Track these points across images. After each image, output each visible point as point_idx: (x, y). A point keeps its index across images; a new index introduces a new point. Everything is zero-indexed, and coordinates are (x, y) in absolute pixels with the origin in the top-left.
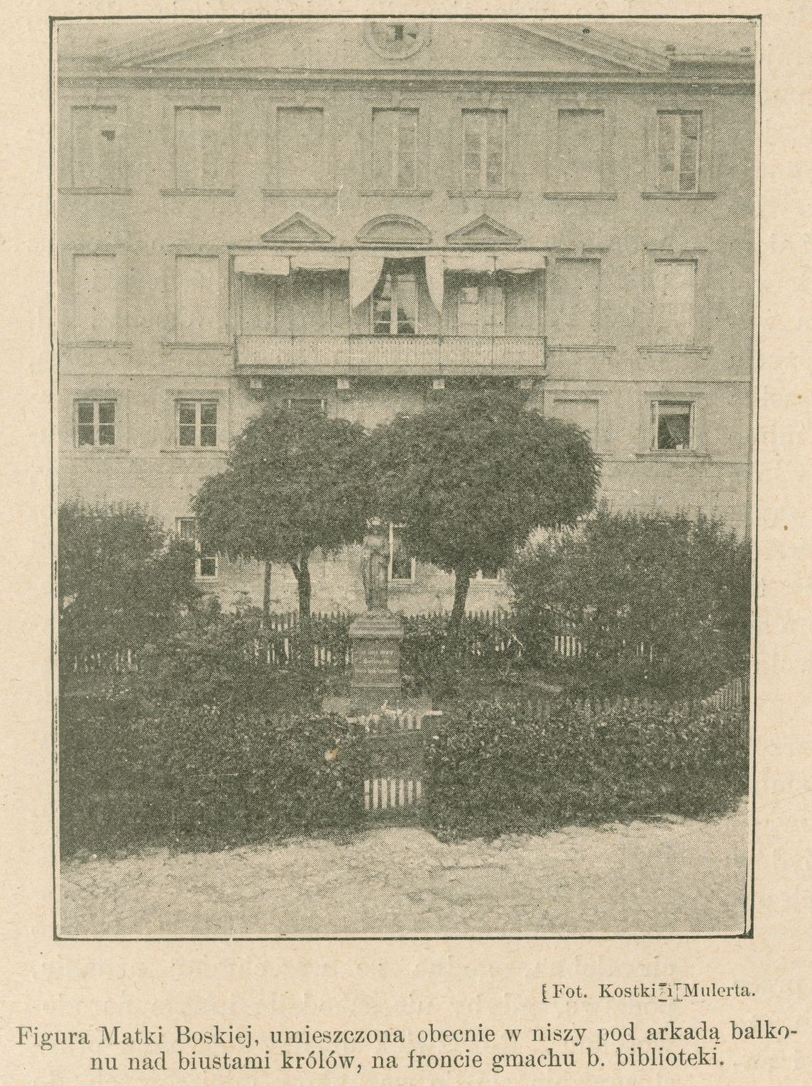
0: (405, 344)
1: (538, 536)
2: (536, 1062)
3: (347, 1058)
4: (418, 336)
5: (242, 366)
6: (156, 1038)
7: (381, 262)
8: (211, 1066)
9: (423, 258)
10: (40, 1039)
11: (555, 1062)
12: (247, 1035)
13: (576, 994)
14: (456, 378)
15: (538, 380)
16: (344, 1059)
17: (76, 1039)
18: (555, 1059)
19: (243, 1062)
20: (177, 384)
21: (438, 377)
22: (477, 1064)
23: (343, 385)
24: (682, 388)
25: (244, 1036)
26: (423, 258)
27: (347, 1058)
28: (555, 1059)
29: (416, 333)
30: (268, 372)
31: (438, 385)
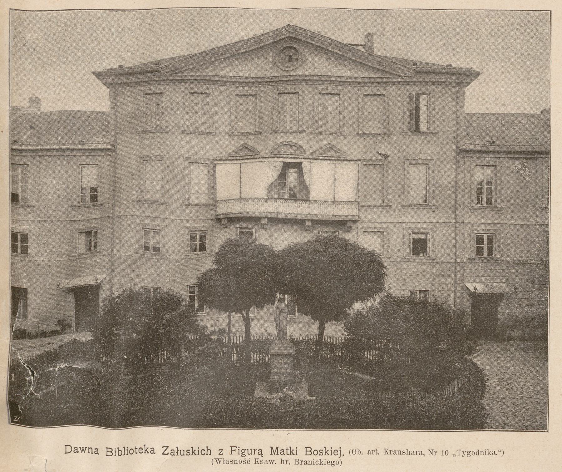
0: (292, 204)
1: (357, 306)
2: (238, 462)
3: (219, 459)
4: (298, 200)
5: (218, 215)
6: (294, 452)
7: (281, 164)
8: (401, 453)
9: (301, 163)
10: (241, 453)
11: (283, 463)
12: (339, 451)
14: (316, 220)
15: (355, 222)
16: (217, 460)
17: (418, 453)
18: (408, 452)
19: (397, 452)
20: (188, 225)
21: (309, 220)
22: (249, 462)
23: (264, 221)
24: (422, 226)
25: (337, 452)
26: (301, 163)
27: (219, 459)
28: (408, 452)
29: (298, 198)
30: (228, 216)
31: (308, 224)
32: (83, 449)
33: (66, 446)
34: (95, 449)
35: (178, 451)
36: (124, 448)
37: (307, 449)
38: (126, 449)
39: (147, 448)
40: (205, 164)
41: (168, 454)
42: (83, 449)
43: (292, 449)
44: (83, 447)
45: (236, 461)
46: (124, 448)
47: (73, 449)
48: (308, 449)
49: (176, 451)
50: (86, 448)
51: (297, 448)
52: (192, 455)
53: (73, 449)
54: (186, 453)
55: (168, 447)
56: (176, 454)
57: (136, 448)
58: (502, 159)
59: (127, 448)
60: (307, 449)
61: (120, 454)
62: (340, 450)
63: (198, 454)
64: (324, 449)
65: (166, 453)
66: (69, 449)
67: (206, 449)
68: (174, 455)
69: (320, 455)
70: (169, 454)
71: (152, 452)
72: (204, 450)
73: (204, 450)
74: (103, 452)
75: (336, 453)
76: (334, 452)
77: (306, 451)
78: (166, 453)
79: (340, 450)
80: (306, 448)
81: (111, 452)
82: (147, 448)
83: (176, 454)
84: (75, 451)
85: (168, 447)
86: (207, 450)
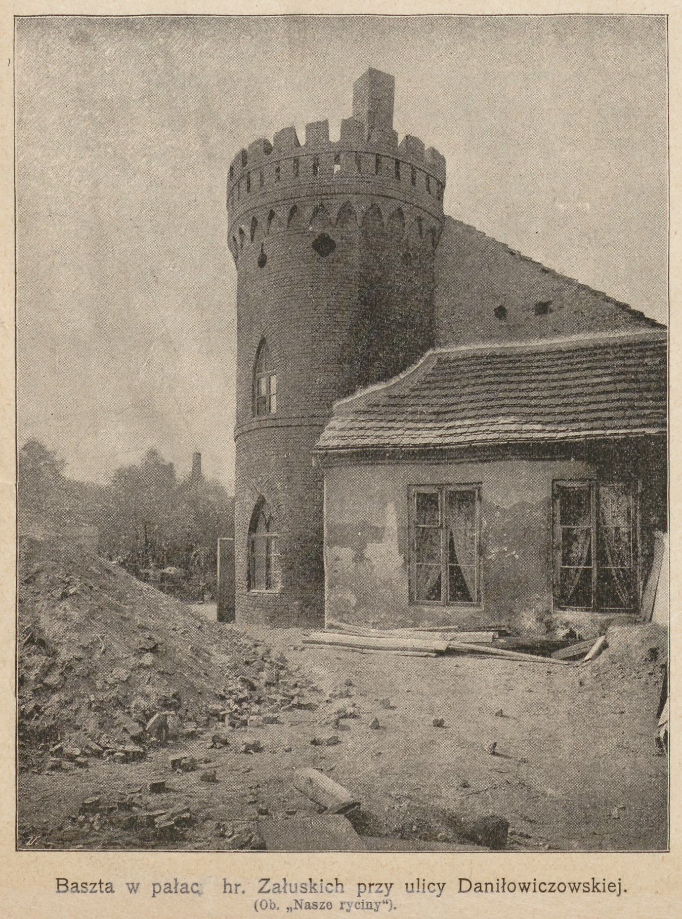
12: (617, 886)
13: (269, 907)
25: (615, 886)
32: (525, 886)
33: (461, 880)
34: (166, 884)
35: (504, 884)
36: (418, 879)
37: (60, 881)
38: (421, 882)
39: (598, 884)
40: (315, 484)
41: (268, 891)
42: (525, 886)
43: (596, 881)
44: (524, 883)
45: (369, 904)
46: (418, 879)
47: (474, 887)
48: (62, 882)
49: (173, 886)
50: (529, 884)
51: (535, 880)
52: (593, 891)
53: (474, 887)
54: (299, 888)
55: (269, 879)
56: (281, 889)
57: (100, 883)
58: (364, 150)
59: (424, 880)
60: (60, 881)
61: (511, 889)
62: (620, 884)
63: (322, 892)
64: (591, 882)
65: (553, 889)
66: (465, 885)
67: (334, 882)
68: (279, 892)
69: (584, 891)
70: (271, 891)
71: (109, 890)
72: (331, 884)
73: (331, 884)
74: (145, 890)
75: (612, 889)
76: (609, 886)
77: (59, 885)
78: (553, 889)
79: (620, 884)
80: (58, 879)
81: (65, 885)
82: (598, 884)
83: (174, 890)
84: (167, 890)
85: (269, 879)
86: (337, 885)
